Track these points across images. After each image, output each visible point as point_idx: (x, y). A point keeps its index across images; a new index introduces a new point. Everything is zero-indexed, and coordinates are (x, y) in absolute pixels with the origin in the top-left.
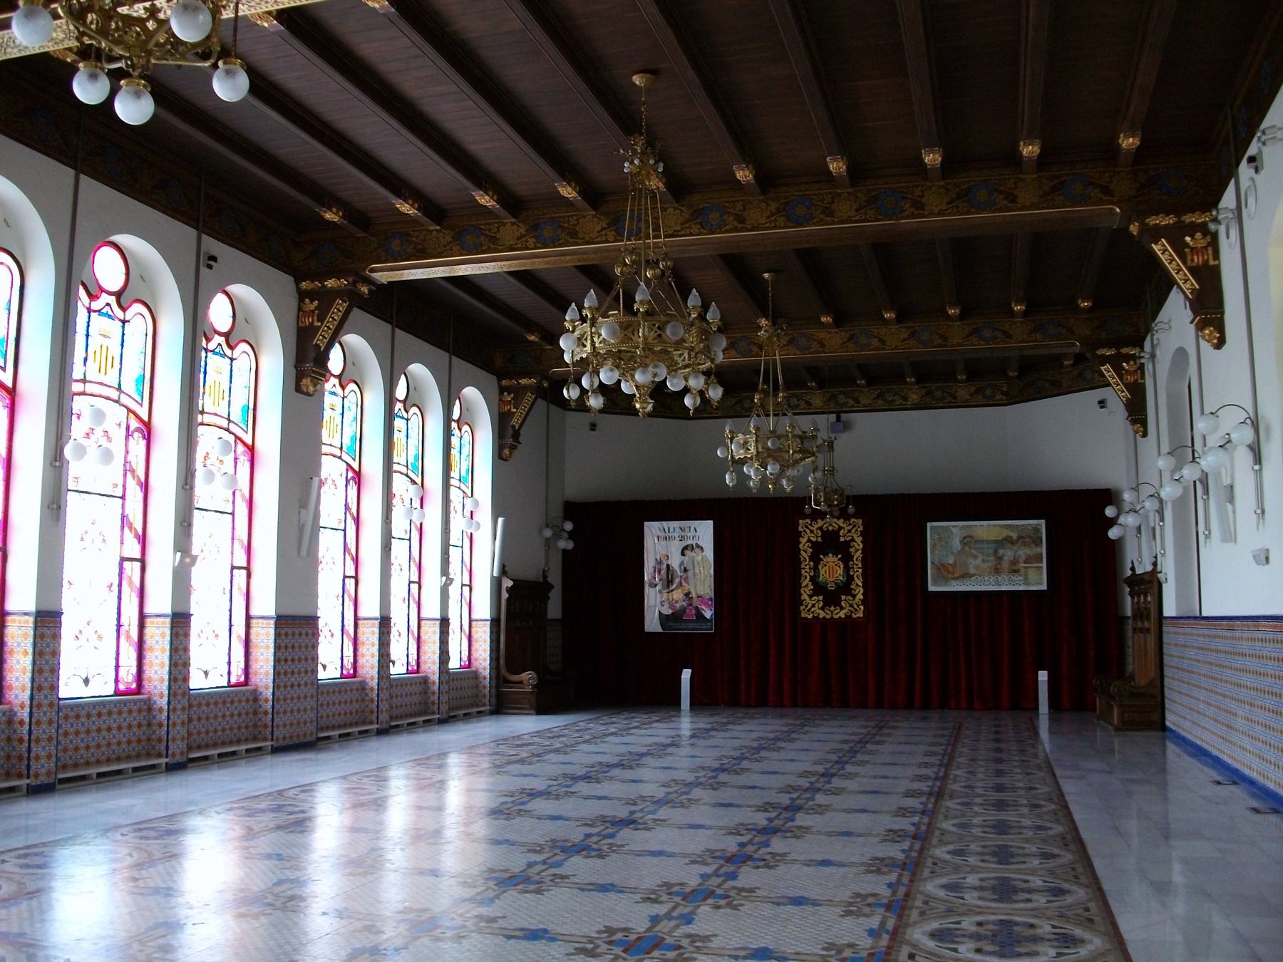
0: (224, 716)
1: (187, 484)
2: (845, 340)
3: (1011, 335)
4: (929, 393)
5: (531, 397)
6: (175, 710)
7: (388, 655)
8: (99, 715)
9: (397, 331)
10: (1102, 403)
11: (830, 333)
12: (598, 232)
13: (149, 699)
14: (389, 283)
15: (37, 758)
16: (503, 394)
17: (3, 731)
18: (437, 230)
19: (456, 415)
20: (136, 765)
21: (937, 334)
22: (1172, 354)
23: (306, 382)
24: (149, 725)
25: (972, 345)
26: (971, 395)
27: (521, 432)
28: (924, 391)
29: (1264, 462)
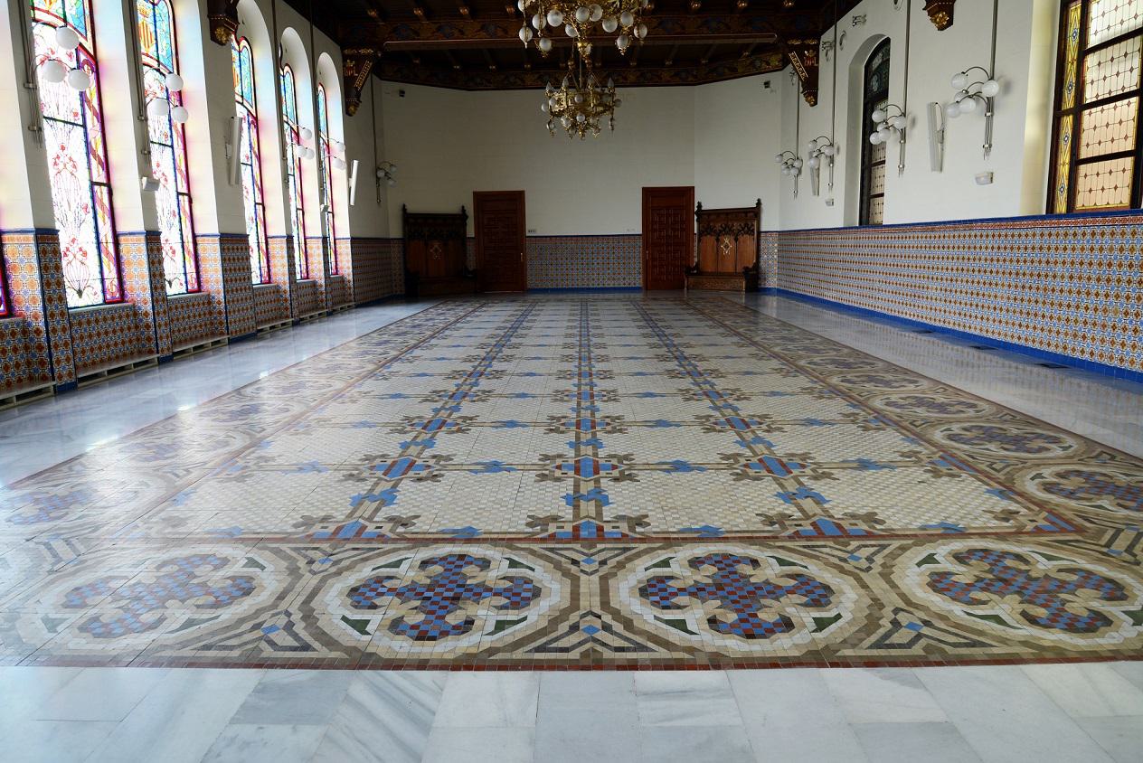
0: (189, 317)
1: (141, 116)
6: (158, 313)
7: (162, 275)
8: (97, 321)
10: (767, 84)
13: (134, 306)
15: (58, 362)
17: (1140, 340)
20: (138, 361)
22: (864, 41)
23: (220, 31)
24: (137, 327)
26: (671, 77)
28: (639, 73)
29: (995, 111)
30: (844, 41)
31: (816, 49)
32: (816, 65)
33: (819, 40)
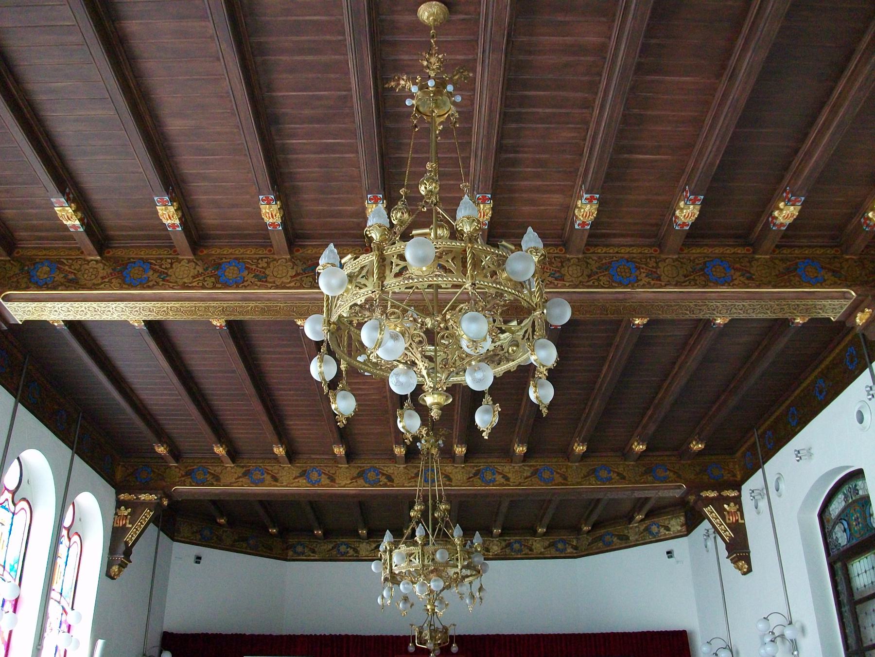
2: (471, 475)
3: (625, 477)
4: (509, 545)
5: (149, 513)
9: (20, 406)
11: (457, 467)
12: (292, 277)
14: (26, 322)
16: (119, 508)
18: (97, 261)
19: (67, 522)
21: (558, 473)
25: (590, 484)
27: (134, 550)
28: (504, 544)
30: (782, 486)
31: (738, 500)
32: (740, 521)
33: (740, 491)
